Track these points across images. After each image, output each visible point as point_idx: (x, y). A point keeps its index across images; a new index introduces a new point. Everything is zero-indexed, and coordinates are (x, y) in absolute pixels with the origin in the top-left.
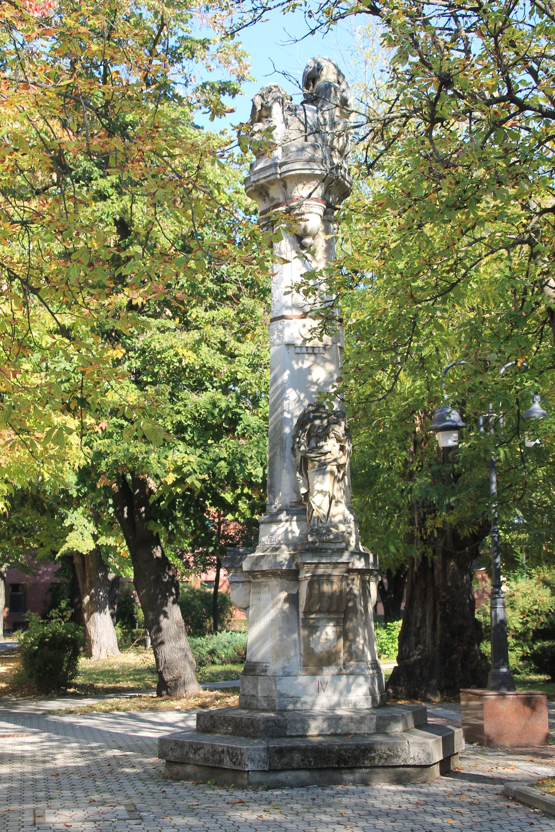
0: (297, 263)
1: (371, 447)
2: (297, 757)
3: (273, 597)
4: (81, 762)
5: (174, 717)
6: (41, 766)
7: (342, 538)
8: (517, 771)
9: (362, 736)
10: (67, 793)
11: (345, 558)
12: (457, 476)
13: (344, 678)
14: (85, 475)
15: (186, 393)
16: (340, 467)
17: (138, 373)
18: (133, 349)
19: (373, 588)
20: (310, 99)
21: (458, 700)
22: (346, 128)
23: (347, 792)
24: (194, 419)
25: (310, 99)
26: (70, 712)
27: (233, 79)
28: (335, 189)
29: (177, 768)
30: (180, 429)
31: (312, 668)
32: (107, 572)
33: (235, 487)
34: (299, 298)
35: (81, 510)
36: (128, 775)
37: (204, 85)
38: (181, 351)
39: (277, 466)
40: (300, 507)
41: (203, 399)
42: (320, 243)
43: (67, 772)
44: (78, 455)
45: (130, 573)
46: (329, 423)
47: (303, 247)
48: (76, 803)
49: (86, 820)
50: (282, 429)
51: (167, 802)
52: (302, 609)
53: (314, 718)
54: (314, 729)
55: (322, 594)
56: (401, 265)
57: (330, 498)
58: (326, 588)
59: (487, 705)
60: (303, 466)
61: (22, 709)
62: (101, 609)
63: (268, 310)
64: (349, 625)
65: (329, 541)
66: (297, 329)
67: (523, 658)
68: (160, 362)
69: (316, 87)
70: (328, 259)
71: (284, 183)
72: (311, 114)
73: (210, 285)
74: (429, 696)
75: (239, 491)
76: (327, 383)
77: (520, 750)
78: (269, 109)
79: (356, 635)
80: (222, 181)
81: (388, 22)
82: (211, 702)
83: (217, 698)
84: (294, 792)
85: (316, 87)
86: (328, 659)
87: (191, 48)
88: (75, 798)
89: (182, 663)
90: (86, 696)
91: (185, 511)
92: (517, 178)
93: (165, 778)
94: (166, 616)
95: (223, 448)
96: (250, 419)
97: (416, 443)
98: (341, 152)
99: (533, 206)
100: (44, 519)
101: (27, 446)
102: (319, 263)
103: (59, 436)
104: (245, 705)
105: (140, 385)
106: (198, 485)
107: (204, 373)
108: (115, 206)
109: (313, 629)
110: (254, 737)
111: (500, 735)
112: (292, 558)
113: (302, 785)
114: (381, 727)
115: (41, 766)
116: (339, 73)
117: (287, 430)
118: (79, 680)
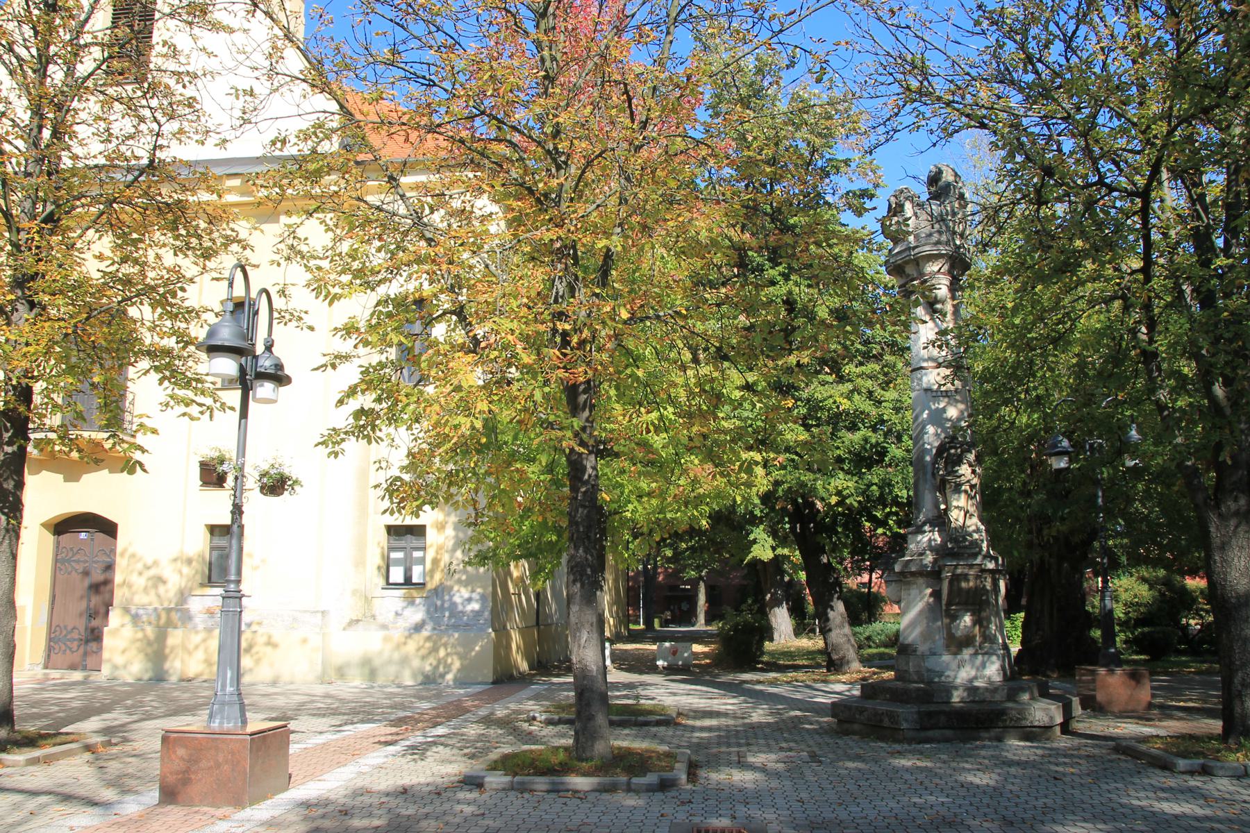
0: (931, 324)
1: (995, 471)
2: (943, 718)
3: (921, 592)
4: (771, 719)
5: (842, 687)
6: (741, 721)
7: (976, 544)
8: (1126, 731)
9: (996, 702)
10: (762, 741)
11: (978, 561)
12: (1068, 492)
13: (980, 657)
14: (767, 498)
15: (843, 433)
16: (972, 487)
17: (805, 418)
18: (800, 399)
19: (1002, 584)
20: (934, 196)
21: (1073, 676)
22: (965, 216)
23: (984, 747)
24: (850, 452)
25: (934, 196)
26: (759, 682)
27: (870, 187)
28: (958, 264)
29: (846, 726)
30: (839, 460)
31: (953, 649)
32: (783, 577)
33: (885, 506)
34: (935, 352)
35: (762, 527)
36: (808, 730)
37: (848, 193)
38: (838, 399)
39: (921, 488)
40: (940, 521)
41: (857, 436)
42: (949, 307)
43: (760, 726)
44: (762, 481)
45: (803, 576)
46: (962, 452)
47: (935, 311)
48: (769, 749)
49: (777, 762)
50: (923, 458)
51: (840, 752)
52: (944, 602)
53: (956, 688)
54: (956, 697)
55: (960, 589)
56: (1017, 321)
57: (963, 511)
58: (964, 585)
59: (1098, 678)
60: (942, 486)
61: (723, 679)
62: (779, 604)
63: (907, 364)
64: (984, 614)
65: (966, 547)
66: (933, 377)
67: (1126, 642)
68: (821, 409)
69: (938, 187)
70: (955, 320)
71: (919, 262)
72: (935, 208)
73: (859, 347)
74: (1049, 673)
75: (888, 510)
76: (959, 419)
77: (1125, 715)
78: (902, 206)
79: (989, 622)
80: (865, 265)
81: (995, 132)
82: (870, 677)
83: (875, 673)
84: (941, 746)
85: (938, 187)
86: (967, 641)
87: (835, 167)
88: (768, 745)
89: (847, 646)
90: (771, 671)
91: (845, 526)
92: (1110, 245)
93: (837, 733)
94: (832, 609)
95: (875, 476)
96: (895, 451)
97: (1032, 467)
98: (962, 235)
99: (1124, 268)
100: (735, 533)
101: (725, 476)
102: (949, 323)
103: (748, 467)
104: (897, 678)
105: (807, 427)
106: (856, 504)
107: (858, 417)
108: (781, 290)
109: (954, 617)
110: (907, 703)
111: (1110, 702)
112: (935, 561)
113: (947, 740)
114: (1012, 696)
115: (741, 721)
116: (956, 175)
117: (928, 458)
118: (765, 658)
